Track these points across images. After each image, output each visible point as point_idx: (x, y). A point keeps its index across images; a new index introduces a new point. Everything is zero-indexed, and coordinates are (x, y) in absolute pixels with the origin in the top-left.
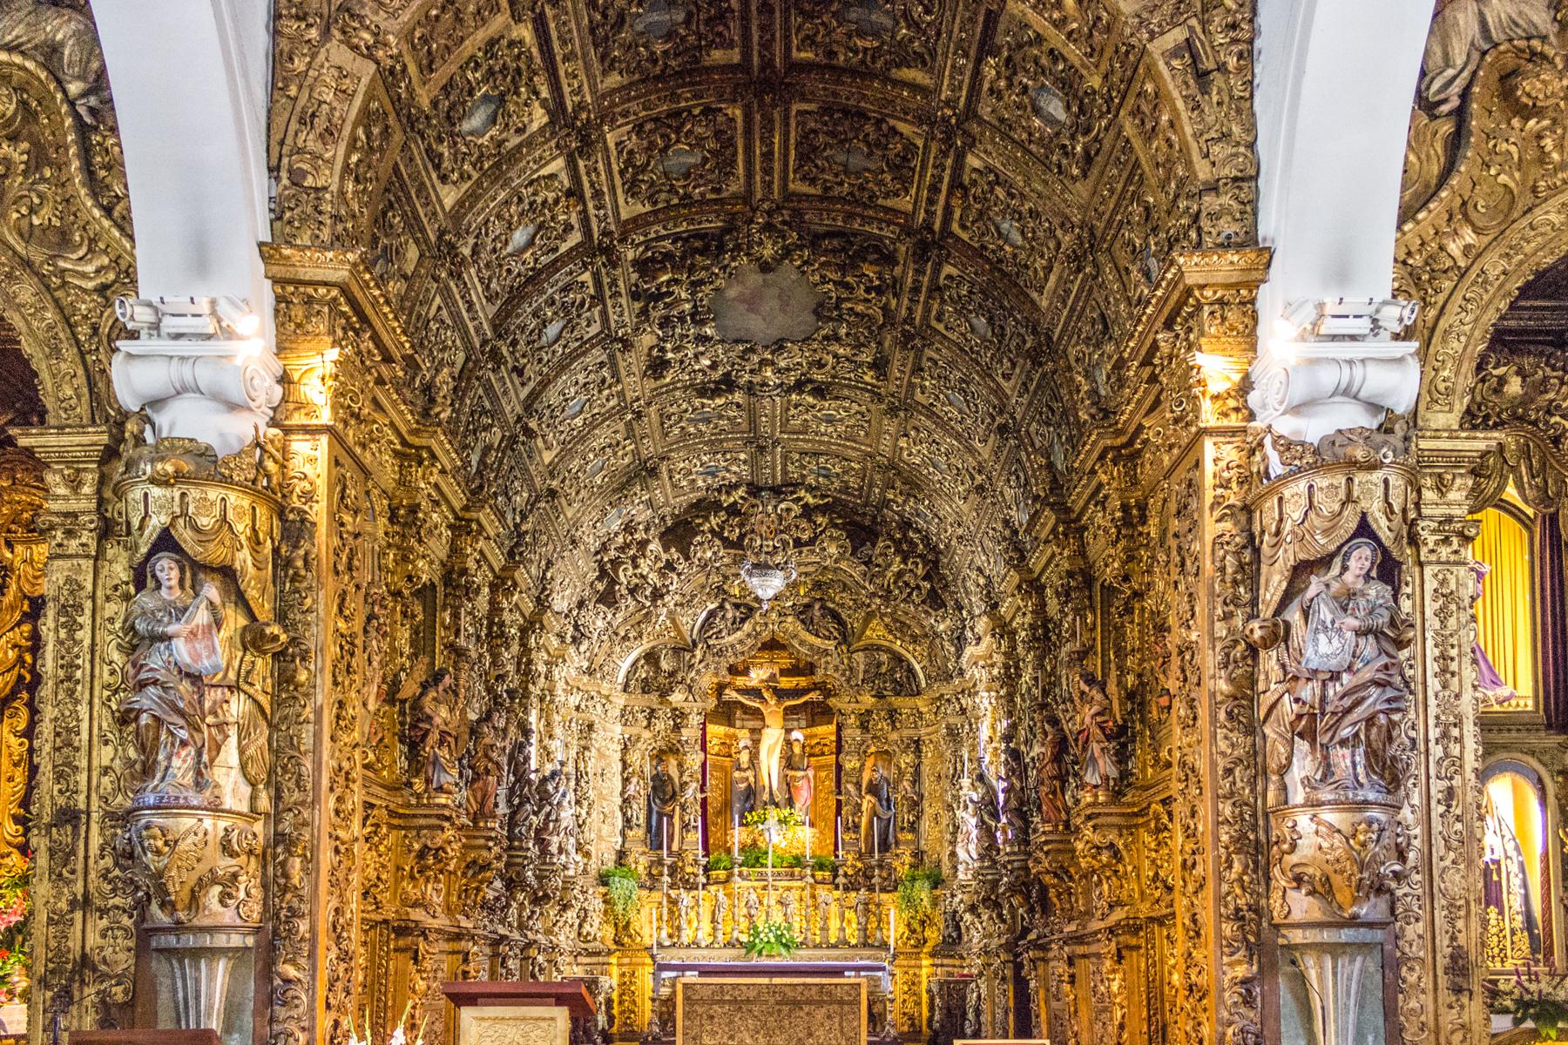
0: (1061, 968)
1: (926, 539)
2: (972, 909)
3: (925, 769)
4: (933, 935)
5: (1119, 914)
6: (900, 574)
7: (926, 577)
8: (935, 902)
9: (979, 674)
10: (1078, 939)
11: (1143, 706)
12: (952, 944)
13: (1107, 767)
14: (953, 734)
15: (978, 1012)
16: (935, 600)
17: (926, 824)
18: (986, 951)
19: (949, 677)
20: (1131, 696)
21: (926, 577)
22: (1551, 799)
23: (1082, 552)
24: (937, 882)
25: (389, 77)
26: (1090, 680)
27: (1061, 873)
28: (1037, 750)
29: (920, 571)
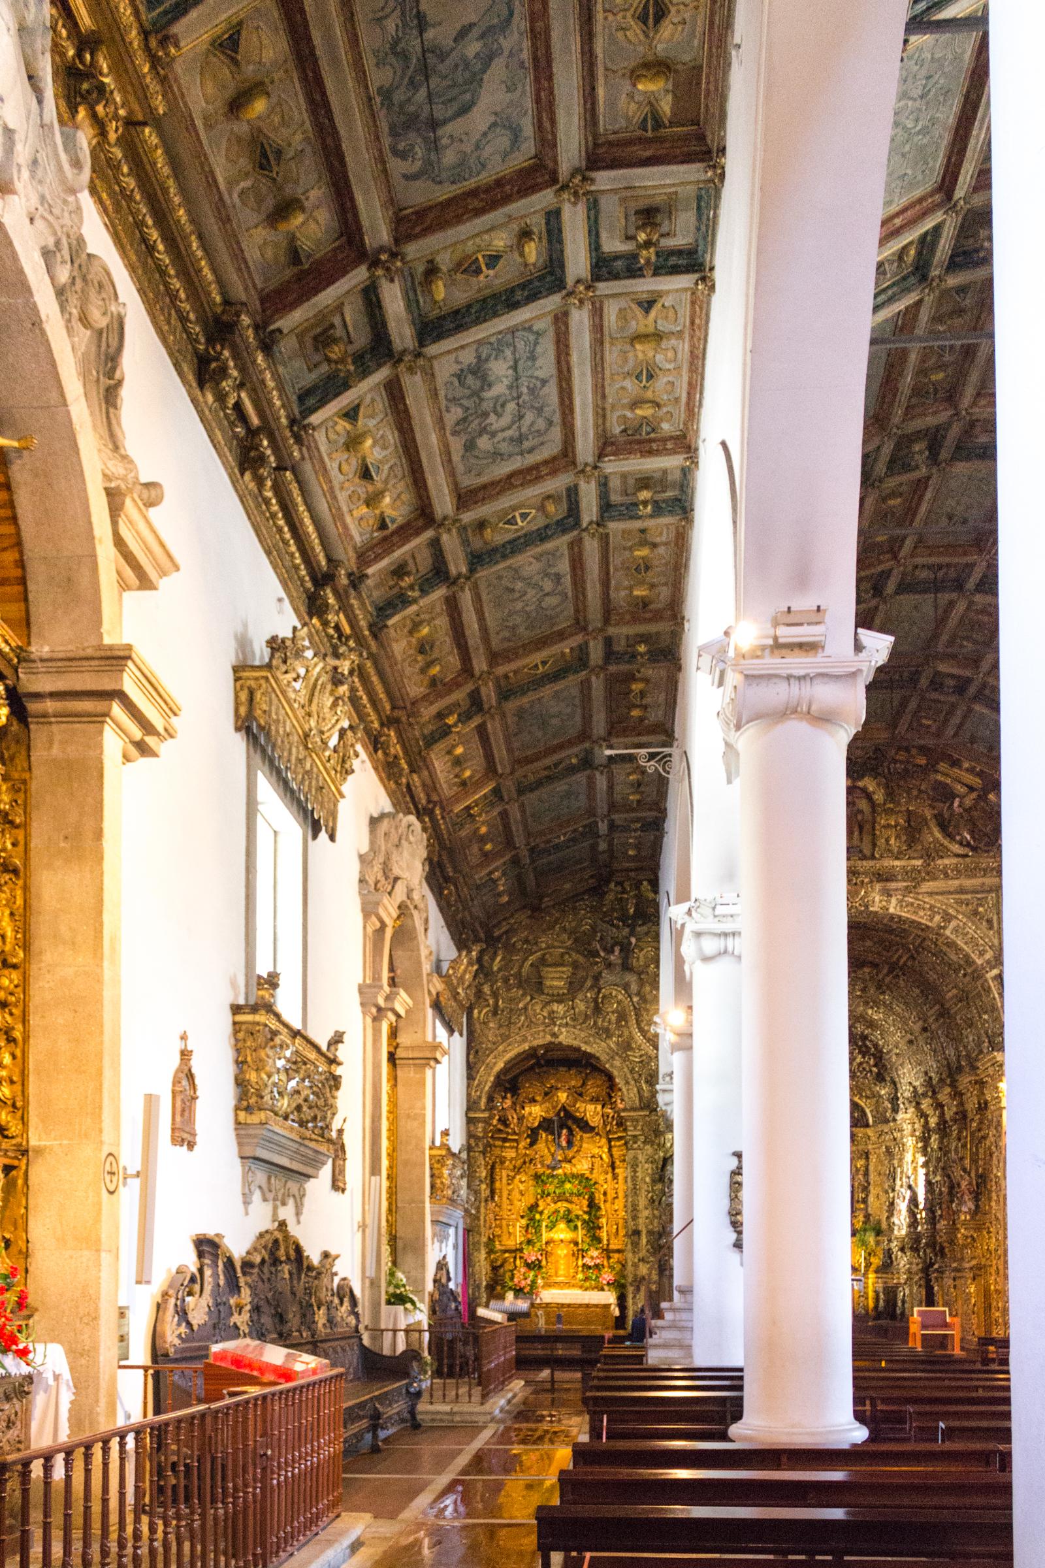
0: (951, 1282)
1: (876, 1046)
2: (902, 1249)
3: (871, 1168)
4: (876, 1261)
5: (974, 1262)
6: (861, 1064)
7: (875, 1065)
8: (878, 1243)
9: (907, 1128)
10: (957, 1270)
11: (985, 1182)
12: (887, 1266)
13: (971, 1205)
14: (889, 1152)
15: (903, 1302)
16: (880, 1078)
17: (871, 1199)
18: (909, 1271)
19: (887, 1121)
20: (981, 1176)
21: (875, 1065)
22: (866, 515)
23: (962, 1104)
24: (878, 1232)
25: (466, 1211)
26: (964, 1170)
27: (952, 1242)
28: (938, 1178)
29: (872, 1062)
